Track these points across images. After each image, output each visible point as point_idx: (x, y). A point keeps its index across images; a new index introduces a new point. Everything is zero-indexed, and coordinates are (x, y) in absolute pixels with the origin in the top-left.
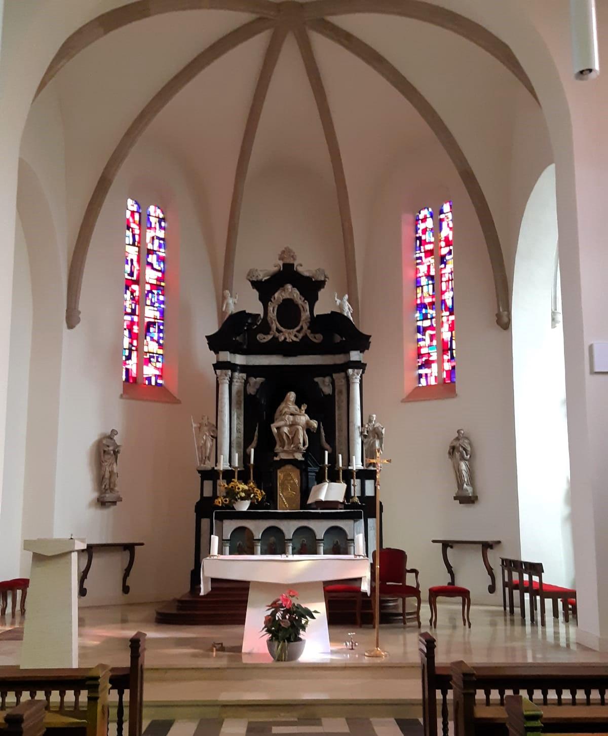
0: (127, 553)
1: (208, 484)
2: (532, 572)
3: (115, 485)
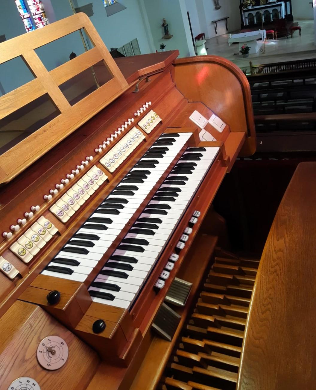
0: (226, 21)
2: (288, 27)
3: (219, 3)
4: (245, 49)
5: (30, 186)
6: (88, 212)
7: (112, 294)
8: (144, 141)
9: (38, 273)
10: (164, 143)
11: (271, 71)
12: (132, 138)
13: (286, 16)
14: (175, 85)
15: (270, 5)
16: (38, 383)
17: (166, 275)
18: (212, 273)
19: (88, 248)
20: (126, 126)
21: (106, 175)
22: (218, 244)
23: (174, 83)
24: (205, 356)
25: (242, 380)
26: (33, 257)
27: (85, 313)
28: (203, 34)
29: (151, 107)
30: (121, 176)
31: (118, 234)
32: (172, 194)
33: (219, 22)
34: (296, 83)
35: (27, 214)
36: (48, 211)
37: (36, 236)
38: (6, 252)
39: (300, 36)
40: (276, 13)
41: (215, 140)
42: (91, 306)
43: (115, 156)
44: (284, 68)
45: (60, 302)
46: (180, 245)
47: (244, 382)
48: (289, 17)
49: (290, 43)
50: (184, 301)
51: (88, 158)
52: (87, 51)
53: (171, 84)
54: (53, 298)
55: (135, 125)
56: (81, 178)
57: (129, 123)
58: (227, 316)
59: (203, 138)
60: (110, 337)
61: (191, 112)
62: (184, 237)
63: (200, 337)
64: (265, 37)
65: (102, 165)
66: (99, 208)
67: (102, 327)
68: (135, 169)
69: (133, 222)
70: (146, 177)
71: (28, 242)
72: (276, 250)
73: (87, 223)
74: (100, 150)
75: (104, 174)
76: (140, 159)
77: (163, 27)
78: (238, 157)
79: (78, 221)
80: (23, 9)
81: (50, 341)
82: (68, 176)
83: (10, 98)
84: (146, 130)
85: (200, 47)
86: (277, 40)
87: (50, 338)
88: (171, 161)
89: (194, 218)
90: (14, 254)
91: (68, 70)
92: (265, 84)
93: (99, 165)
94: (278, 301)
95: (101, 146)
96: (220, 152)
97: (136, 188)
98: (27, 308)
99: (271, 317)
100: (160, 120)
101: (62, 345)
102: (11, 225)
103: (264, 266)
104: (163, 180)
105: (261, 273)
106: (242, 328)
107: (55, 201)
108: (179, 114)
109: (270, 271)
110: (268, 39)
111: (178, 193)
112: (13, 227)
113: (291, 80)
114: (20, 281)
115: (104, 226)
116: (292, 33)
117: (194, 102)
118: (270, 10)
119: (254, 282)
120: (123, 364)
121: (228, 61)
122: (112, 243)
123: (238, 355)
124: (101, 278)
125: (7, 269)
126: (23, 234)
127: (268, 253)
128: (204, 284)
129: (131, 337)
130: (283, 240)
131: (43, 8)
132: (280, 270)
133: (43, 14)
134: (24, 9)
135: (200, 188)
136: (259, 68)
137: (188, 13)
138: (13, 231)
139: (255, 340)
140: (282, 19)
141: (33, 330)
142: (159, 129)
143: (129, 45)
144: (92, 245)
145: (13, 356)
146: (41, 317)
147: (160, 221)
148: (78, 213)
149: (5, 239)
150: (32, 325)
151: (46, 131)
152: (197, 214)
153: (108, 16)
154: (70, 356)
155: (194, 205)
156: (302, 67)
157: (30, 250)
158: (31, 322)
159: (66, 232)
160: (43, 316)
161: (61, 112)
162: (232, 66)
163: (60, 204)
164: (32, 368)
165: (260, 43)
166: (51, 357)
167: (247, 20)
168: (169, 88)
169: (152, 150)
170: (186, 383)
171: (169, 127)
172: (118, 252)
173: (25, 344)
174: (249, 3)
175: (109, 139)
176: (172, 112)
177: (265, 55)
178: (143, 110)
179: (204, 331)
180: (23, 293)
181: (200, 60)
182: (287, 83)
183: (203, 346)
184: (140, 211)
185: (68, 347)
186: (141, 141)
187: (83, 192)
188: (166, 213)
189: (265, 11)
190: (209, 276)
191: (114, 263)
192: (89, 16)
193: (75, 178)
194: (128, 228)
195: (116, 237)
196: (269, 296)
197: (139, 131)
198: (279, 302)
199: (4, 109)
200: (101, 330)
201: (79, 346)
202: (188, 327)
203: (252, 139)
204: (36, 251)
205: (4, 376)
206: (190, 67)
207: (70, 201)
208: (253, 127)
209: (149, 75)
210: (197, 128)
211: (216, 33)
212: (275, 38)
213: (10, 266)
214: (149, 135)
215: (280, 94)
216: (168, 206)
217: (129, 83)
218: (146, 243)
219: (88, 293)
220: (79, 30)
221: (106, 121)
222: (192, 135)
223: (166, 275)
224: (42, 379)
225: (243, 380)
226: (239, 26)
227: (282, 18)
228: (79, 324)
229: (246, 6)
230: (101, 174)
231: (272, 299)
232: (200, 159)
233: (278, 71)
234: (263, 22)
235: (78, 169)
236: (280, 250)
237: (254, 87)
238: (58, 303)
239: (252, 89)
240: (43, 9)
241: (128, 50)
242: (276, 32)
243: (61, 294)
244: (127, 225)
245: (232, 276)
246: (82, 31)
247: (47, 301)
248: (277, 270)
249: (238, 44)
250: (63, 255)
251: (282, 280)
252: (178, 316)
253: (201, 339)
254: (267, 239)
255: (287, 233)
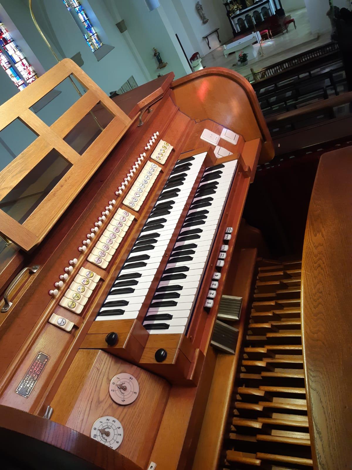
1: (228, 7)
2: (281, 22)
4: (243, 57)
5: (62, 242)
6: (124, 254)
7: (165, 323)
8: (161, 173)
9: (92, 320)
10: (182, 169)
11: (274, 72)
12: (148, 172)
13: (277, 11)
14: (179, 109)
15: (257, 4)
16: (118, 419)
17: (213, 294)
18: (259, 284)
19: (133, 287)
20: (139, 162)
21: (133, 214)
22: (258, 255)
23: (177, 107)
24: (270, 360)
25: (309, 374)
26: (83, 307)
27: (145, 346)
28: (197, 53)
29: (160, 137)
30: (147, 212)
31: (158, 267)
32: (201, 218)
33: (209, 36)
34: (303, 78)
35: (67, 269)
36: (86, 262)
37: (81, 287)
38: (56, 309)
39: (296, 29)
40: (266, 11)
41: (231, 154)
42: (149, 339)
43: (137, 194)
44: (287, 66)
45: (119, 342)
46: (220, 263)
47: (311, 375)
48: (280, 12)
49: (287, 38)
50: (238, 315)
51: (110, 202)
52: (82, 96)
53: (174, 109)
54: (112, 340)
55: (149, 158)
56: (109, 223)
57: (142, 158)
58: (282, 319)
59: (219, 154)
60: (173, 363)
61: (201, 132)
62: (222, 255)
63: (261, 344)
64: (260, 38)
65: (126, 206)
66: (134, 248)
67: (164, 355)
68: (158, 202)
69: (169, 253)
70: (172, 208)
71: (75, 295)
72: (316, 245)
73: (126, 264)
74: (120, 192)
75: (130, 214)
76: (161, 191)
77: (156, 57)
78: (258, 165)
79: (117, 264)
80: (15, 77)
81: (119, 379)
82: (96, 224)
83: (19, 162)
84: (160, 161)
85: (198, 67)
86: (273, 38)
87: (118, 376)
88: (192, 186)
89: (228, 235)
90: (65, 308)
91: (67, 121)
92: (271, 87)
93: (123, 207)
94: (328, 293)
95: (120, 188)
96: (239, 164)
97: (165, 220)
98: (90, 354)
99: (324, 310)
100: (172, 148)
101: (131, 380)
102: (55, 283)
103: (307, 264)
104: (189, 206)
105: (305, 271)
106: (298, 327)
107: (90, 251)
108: (189, 137)
109: (314, 268)
110: (263, 41)
111: (206, 215)
112: (57, 284)
113: (296, 76)
114: (78, 331)
115: (143, 262)
116: (286, 28)
117: (201, 121)
118: (259, 10)
119: (300, 282)
120: (192, 384)
121: (226, 70)
122: (154, 276)
123: (300, 352)
124: (152, 311)
125: (62, 324)
126: (68, 288)
127: (308, 251)
128: (253, 295)
129: (193, 357)
130: (321, 234)
131: (34, 70)
132: (324, 263)
133: (35, 76)
134: (16, 76)
135: (227, 205)
136: (262, 73)
137: (176, 35)
138: (58, 288)
139: (313, 335)
140: (273, 15)
141: (101, 373)
142: (173, 157)
143: (127, 85)
144: (136, 283)
145: (88, 400)
146: (105, 359)
147: (195, 246)
148: (115, 257)
149: (53, 296)
150: (99, 368)
151: (63, 186)
152: (230, 230)
153: (98, 61)
154: (141, 388)
155: (225, 223)
156: (305, 59)
157: (79, 301)
158: (97, 365)
159: (108, 276)
160: (106, 359)
161: (73, 164)
162: (230, 73)
163: (96, 252)
164: (108, 407)
165: (257, 46)
166: (123, 393)
167: (238, 26)
168: (173, 114)
169: (170, 179)
170: (258, 389)
171: (181, 153)
172: (163, 284)
173: (96, 386)
174: (235, 8)
175: (126, 179)
176: (182, 136)
177: (264, 57)
178: (152, 142)
179: (263, 338)
180: (83, 342)
181: (197, 76)
182: (293, 81)
183: (266, 352)
184: (173, 241)
185: (137, 380)
186: (157, 173)
187: (114, 236)
188: (199, 237)
189: (254, 12)
190: (257, 286)
191: (161, 294)
192: (80, 66)
193: (103, 225)
194: (167, 259)
195: (156, 270)
196: (318, 291)
197: (154, 164)
198: (330, 294)
199: (17, 174)
200: (164, 358)
201: (147, 378)
202: (248, 338)
203: (268, 143)
204: (85, 301)
205: (84, 420)
206: (189, 86)
207: (104, 248)
208: (267, 131)
209: (150, 105)
210: (210, 146)
211: (210, 48)
212: (270, 37)
213: (64, 321)
214: (165, 166)
215: (289, 94)
216: (200, 229)
217: (131, 118)
218: (186, 269)
219: (144, 328)
220: (68, 77)
221: (119, 161)
222: (207, 154)
223: (213, 294)
224: (120, 415)
225: (310, 374)
226: (232, 35)
227: (273, 14)
228: (142, 357)
229: (234, 12)
230: (127, 215)
231: (321, 293)
232: (220, 177)
233: (281, 70)
234: (254, 24)
235: (104, 215)
236: (320, 245)
237: (261, 93)
238: (118, 343)
239: (259, 96)
240: (34, 71)
241: (127, 89)
242: (270, 31)
243: (117, 334)
244: (164, 257)
245: (279, 281)
246: (71, 77)
247: (107, 344)
248: (320, 264)
249: (234, 54)
250: (111, 298)
251: (328, 272)
252: (236, 330)
253: (262, 346)
254: (305, 238)
255: (323, 227)
